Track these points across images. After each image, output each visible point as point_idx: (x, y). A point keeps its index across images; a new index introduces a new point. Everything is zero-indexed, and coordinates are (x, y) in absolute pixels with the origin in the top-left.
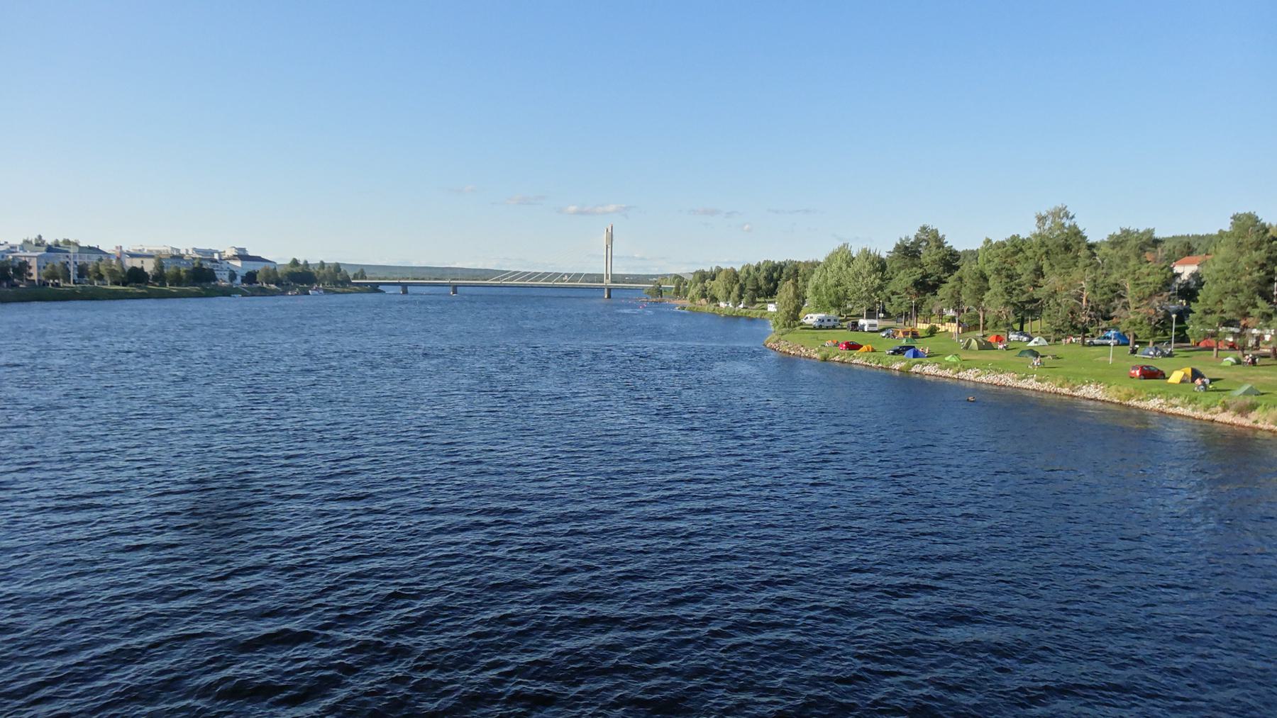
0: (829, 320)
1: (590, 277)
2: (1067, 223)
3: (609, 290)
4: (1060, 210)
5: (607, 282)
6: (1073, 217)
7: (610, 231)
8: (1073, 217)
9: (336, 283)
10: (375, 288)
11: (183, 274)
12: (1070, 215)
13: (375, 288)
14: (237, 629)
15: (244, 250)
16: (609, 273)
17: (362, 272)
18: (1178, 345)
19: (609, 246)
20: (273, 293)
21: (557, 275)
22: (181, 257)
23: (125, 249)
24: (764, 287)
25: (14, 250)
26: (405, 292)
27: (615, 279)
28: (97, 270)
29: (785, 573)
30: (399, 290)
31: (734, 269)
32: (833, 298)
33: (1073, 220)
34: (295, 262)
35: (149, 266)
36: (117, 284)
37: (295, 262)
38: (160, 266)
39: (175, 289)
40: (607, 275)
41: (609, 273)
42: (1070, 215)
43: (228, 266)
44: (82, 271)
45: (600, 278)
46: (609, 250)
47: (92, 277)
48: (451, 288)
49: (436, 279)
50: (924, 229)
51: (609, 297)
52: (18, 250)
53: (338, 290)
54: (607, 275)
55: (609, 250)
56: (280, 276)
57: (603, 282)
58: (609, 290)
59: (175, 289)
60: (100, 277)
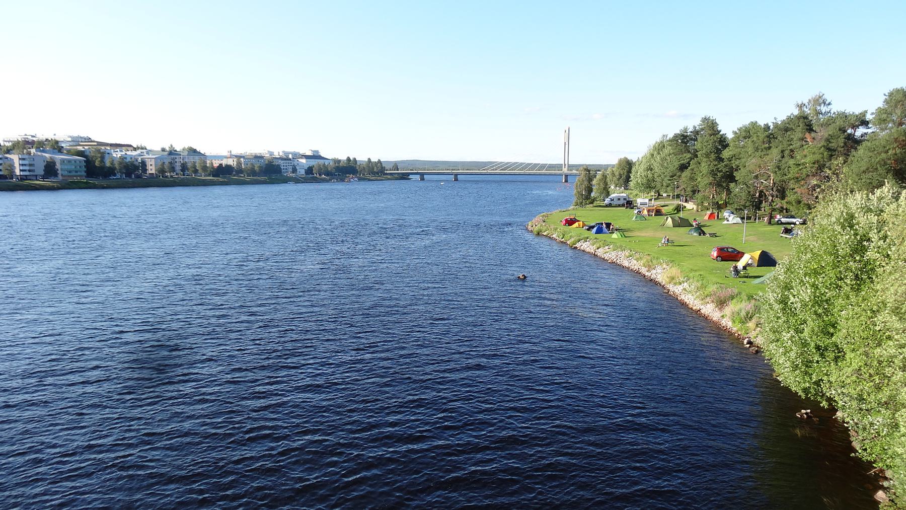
0: (619, 199)
1: (551, 167)
2: (824, 109)
3: (566, 176)
4: (820, 97)
5: (565, 170)
6: (829, 104)
7: (567, 132)
8: (829, 104)
9: (374, 173)
10: (404, 177)
11: (256, 168)
12: (827, 103)
13: (404, 177)
14: (575, 394)
15: (317, 152)
16: (566, 163)
17: (396, 166)
18: (748, 221)
19: (567, 143)
20: (324, 181)
21: (536, 165)
22: (262, 157)
23: (233, 153)
24: (18, 172)
25: (142, 154)
26: (422, 179)
27: (571, 167)
28: (194, 167)
29: (720, 393)
30: (418, 177)
31: (626, 158)
32: (645, 181)
33: (829, 107)
34: (349, 159)
35: (231, 162)
36: (209, 175)
37: (349, 159)
38: (239, 163)
39: (248, 179)
40: (565, 165)
41: (566, 163)
42: (827, 103)
43: (298, 162)
44: (184, 167)
45: (559, 167)
46: (567, 146)
47: (190, 171)
48: (453, 176)
49: (468, 170)
50: (705, 120)
51: (566, 181)
52: (145, 154)
53: (373, 178)
54: (565, 165)
55: (567, 146)
56: (329, 169)
57: (562, 170)
58: (566, 176)
59: (248, 179)
60: (196, 171)
